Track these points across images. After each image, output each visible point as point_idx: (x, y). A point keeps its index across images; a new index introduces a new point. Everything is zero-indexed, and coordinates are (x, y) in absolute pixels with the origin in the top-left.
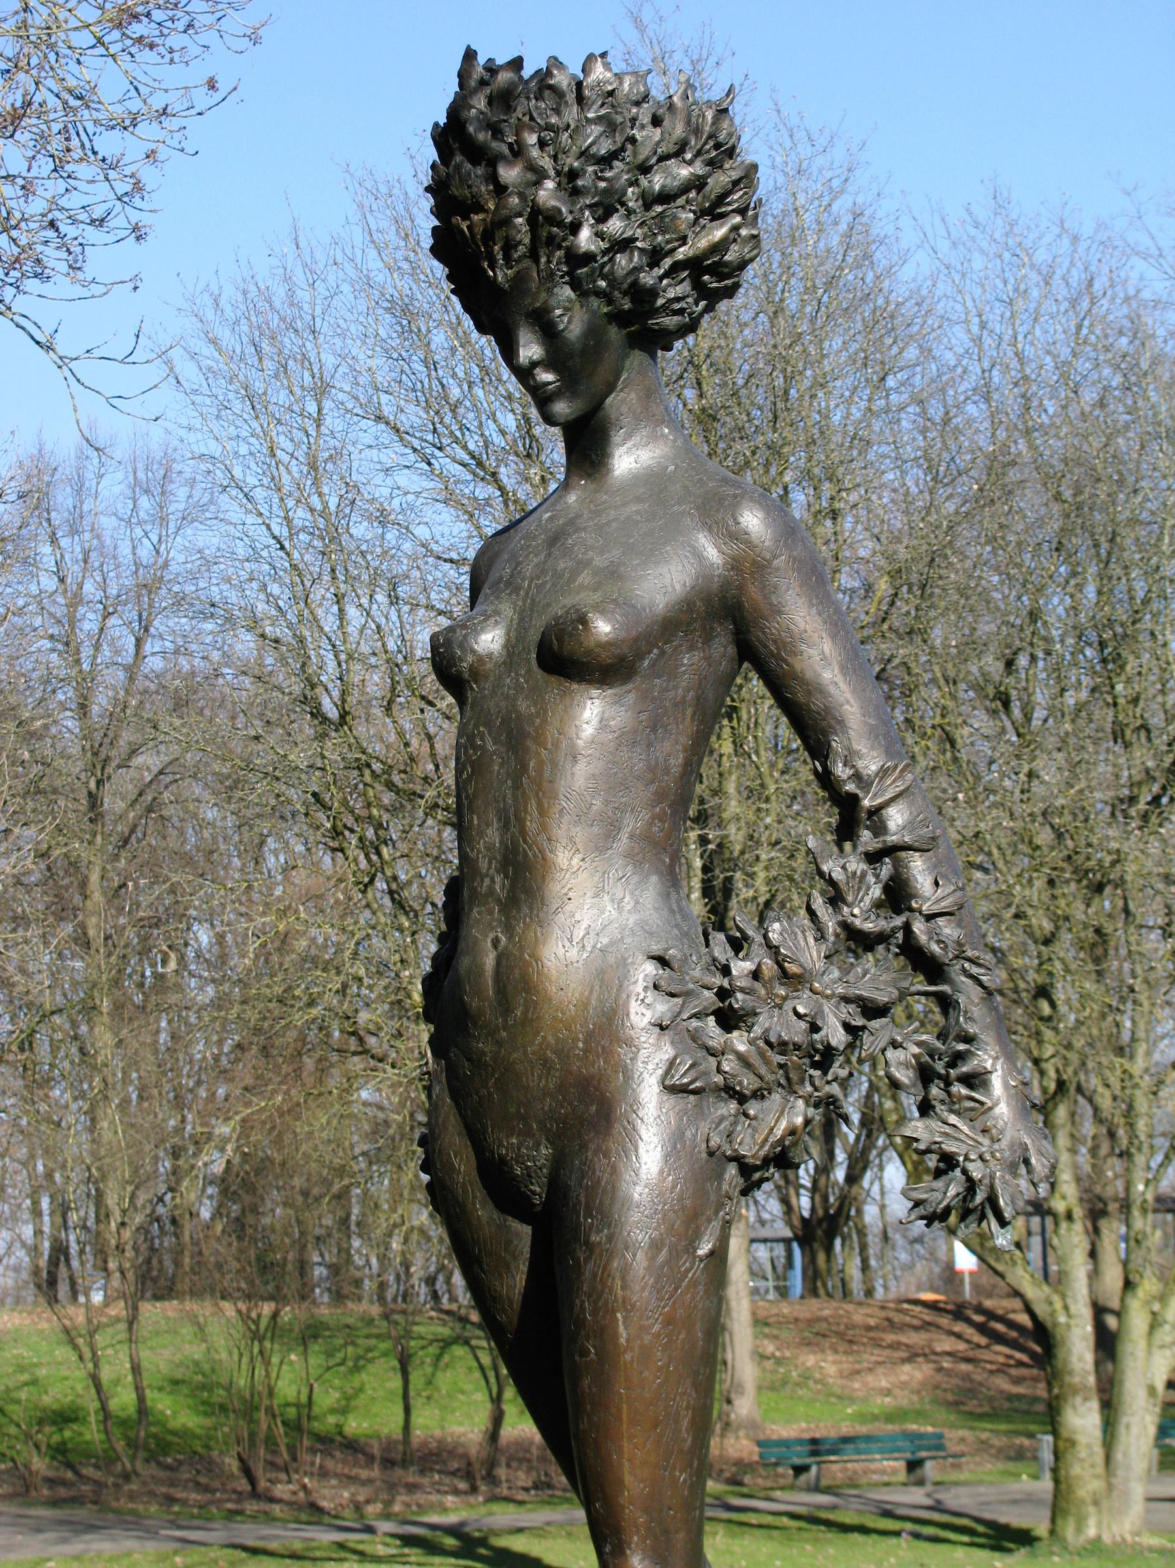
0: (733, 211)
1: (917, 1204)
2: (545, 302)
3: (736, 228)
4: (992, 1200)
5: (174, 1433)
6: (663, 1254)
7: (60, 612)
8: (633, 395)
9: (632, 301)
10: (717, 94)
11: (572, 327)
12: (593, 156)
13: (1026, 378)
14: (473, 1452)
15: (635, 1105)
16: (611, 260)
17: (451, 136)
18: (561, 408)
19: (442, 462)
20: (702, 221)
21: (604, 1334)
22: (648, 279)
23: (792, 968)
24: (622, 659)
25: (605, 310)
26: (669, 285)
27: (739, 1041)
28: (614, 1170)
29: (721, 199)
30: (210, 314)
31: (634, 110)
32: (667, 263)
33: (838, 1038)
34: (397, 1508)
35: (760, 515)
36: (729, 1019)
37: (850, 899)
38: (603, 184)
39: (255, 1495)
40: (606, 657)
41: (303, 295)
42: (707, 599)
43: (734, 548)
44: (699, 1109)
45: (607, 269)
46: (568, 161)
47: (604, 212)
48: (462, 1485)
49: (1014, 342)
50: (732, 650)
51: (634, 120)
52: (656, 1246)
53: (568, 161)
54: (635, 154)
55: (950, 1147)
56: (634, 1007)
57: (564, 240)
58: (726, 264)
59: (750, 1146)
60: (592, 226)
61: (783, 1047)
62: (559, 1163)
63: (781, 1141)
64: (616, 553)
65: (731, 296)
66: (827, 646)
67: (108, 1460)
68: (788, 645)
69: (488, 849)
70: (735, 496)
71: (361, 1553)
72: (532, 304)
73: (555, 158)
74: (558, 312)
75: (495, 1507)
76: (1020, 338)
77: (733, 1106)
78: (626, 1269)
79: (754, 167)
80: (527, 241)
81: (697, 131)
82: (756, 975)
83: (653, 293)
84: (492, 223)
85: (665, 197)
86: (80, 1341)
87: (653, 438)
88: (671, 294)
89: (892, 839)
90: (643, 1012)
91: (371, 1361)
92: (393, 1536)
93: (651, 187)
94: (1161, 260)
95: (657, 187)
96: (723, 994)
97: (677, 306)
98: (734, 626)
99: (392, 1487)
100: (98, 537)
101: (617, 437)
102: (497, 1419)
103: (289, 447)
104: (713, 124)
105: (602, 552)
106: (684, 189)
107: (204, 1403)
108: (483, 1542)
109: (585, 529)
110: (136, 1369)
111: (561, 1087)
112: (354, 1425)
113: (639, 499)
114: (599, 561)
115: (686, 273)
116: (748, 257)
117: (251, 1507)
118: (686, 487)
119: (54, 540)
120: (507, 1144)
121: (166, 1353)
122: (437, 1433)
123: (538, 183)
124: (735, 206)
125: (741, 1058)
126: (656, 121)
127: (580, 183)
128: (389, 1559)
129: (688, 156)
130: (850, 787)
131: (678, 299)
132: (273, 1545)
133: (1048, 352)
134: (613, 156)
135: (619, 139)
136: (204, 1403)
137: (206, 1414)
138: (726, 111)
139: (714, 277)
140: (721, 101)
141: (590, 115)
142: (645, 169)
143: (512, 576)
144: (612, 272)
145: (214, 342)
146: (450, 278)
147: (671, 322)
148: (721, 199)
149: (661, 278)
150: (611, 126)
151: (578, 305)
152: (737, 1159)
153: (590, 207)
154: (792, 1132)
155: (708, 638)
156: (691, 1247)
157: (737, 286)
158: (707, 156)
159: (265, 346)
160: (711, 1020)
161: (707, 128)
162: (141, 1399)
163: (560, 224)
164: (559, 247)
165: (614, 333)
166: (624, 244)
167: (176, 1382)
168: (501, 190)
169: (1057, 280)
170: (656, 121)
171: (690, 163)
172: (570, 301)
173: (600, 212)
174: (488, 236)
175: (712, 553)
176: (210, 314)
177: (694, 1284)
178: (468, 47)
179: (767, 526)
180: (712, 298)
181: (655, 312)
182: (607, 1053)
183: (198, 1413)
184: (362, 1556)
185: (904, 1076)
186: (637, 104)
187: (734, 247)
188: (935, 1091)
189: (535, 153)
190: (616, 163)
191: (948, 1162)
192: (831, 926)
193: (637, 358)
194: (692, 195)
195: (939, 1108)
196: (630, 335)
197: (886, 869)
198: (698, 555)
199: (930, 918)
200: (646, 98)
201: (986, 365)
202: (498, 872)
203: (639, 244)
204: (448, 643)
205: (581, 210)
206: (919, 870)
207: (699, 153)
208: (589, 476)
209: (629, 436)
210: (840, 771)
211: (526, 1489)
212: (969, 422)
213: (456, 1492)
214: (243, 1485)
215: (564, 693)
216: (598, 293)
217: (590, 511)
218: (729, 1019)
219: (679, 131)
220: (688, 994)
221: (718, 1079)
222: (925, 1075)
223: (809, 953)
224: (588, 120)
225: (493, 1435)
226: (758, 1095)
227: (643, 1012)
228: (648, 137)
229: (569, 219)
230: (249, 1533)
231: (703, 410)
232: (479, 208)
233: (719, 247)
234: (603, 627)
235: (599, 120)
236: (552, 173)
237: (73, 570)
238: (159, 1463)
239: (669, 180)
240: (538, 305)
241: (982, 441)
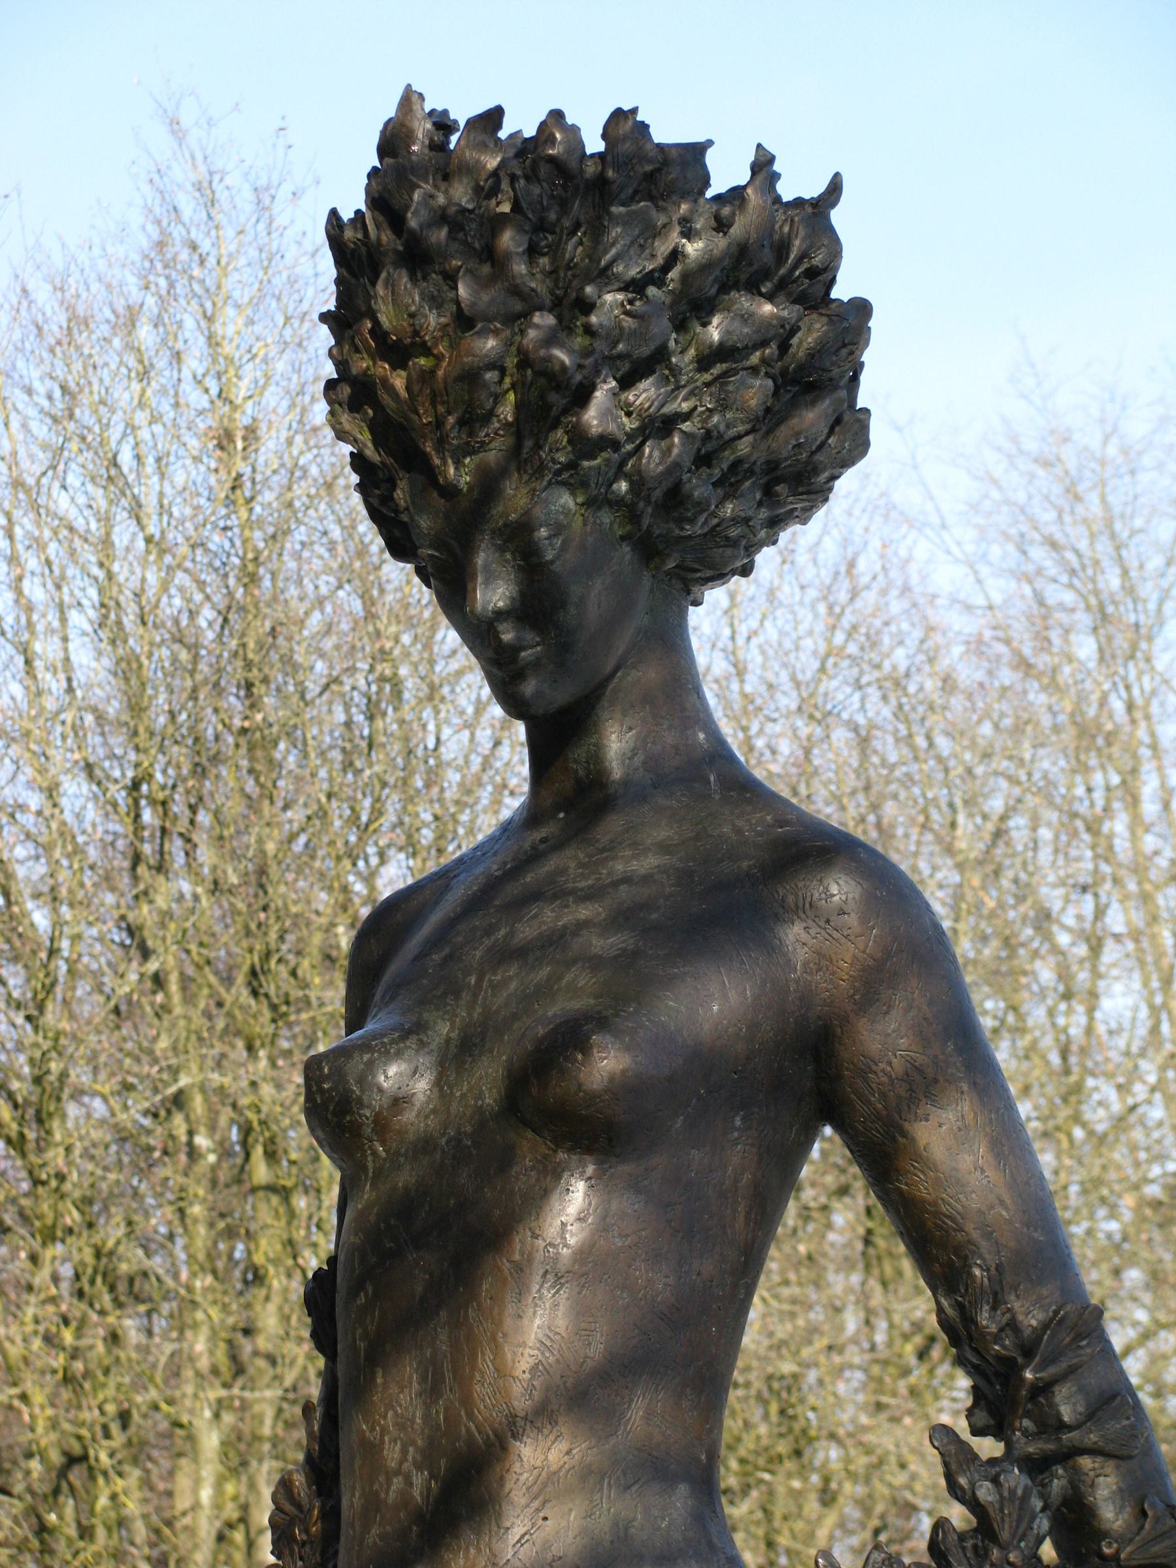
2: (527, 513)
10: (813, 189)
16: (639, 448)
37: (1005, 1535)
69: (401, 1427)
74: (543, 532)
94: (944, 533)
202: (419, 1467)
204: (339, 1074)
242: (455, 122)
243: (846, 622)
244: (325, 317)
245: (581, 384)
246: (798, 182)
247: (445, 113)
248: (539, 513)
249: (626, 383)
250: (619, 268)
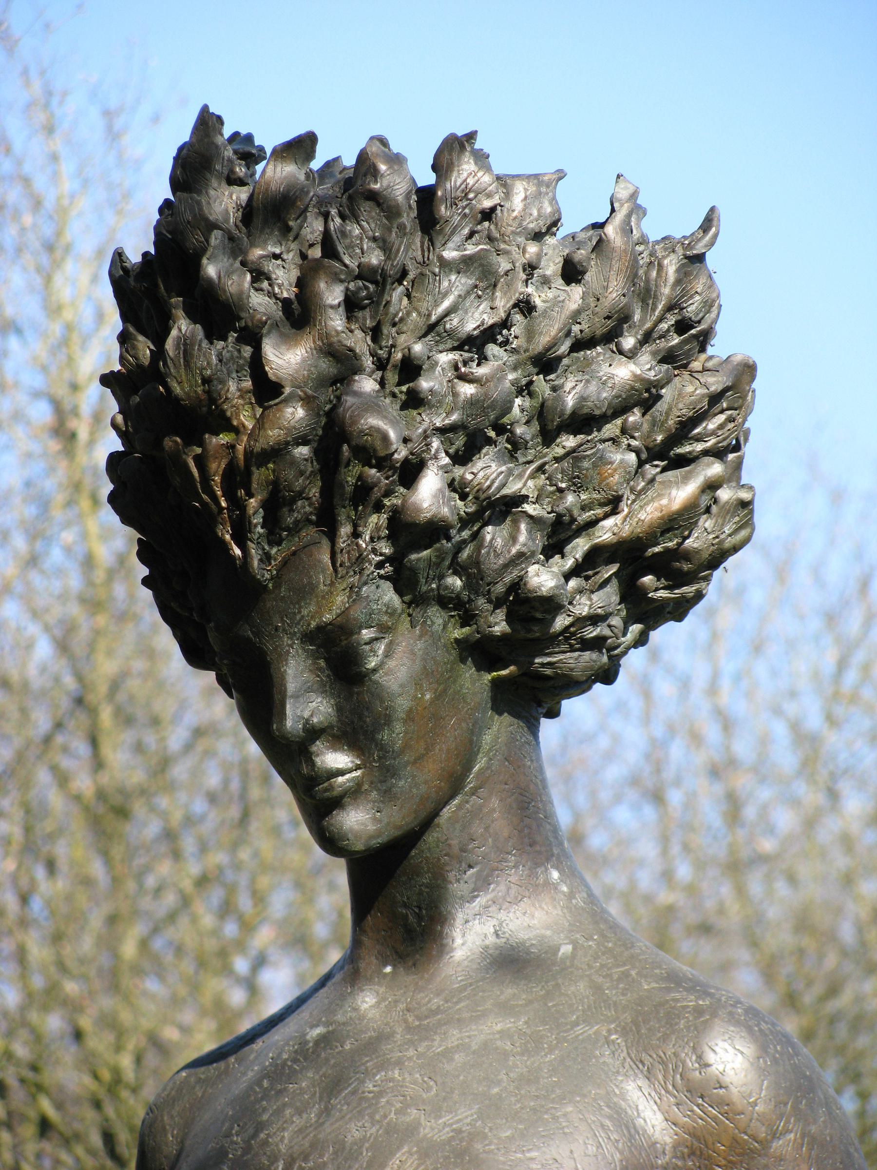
0: (706, 453)
2: (345, 612)
3: (712, 486)
8: (495, 802)
9: (509, 620)
10: (685, 226)
11: (391, 664)
12: (450, 334)
13: (732, 763)
16: (476, 536)
17: (158, 286)
18: (357, 821)
20: (650, 470)
22: (543, 578)
25: (458, 633)
26: (580, 591)
29: (685, 429)
31: (532, 249)
32: (579, 547)
35: (749, 1049)
38: (467, 390)
43: (695, 1114)
45: (465, 554)
46: (402, 339)
47: (468, 443)
49: (713, 690)
51: (531, 268)
53: (402, 339)
54: (530, 334)
57: (388, 493)
58: (687, 556)
60: (445, 470)
64: (464, 1115)
65: (680, 618)
70: (699, 1011)
72: (319, 613)
73: (376, 333)
74: (367, 634)
76: (726, 684)
79: (748, 370)
80: (314, 492)
83: (551, 605)
84: (249, 454)
85: (584, 422)
88: (583, 607)
93: (560, 400)
95: (570, 401)
97: (591, 632)
104: (678, 282)
105: (436, 1112)
109: (399, 1063)
115: (613, 568)
116: (729, 543)
118: (597, 989)
124: (711, 442)
126: (572, 273)
127: (425, 384)
129: (628, 342)
131: (594, 619)
133: (777, 711)
135: (503, 302)
138: (700, 258)
139: (660, 577)
140: (693, 239)
141: (450, 254)
142: (546, 364)
143: (247, 1149)
144: (476, 561)
146: (145, 554)
148: (685, 429)
149: (567, 577)
151: (405, 621)
153: (442, 431)
157: (699, 596)
158: (662, 344)
161: (666, 291)
163: (383, 462)
164: (378, 507)
165: (475, 683)
166: (504, 508)
168: (267, 390)
169: (801, 576)
170: (572, 273)
171: (631, 355)
172: (391, 612)
173: (460, 441)
178: (205, 109)
179: (762, 1072)
180: (648, 614)
181: (548, 642)
186: (538, 236)
187: (706, 523)
190: (492, 349)
194: (635, 417)
196: (497, 685)
198: (625, 1123)
201: (658, 731)
203: (529, 508)
205: (425, 436)
207: (647, 338)
209: (483, 883)
212: (624, 842)
216: (445, 601)
217: (409, 1029)
219: (615, 292)
224: (445, 264)
228: (556, 303)
229: (401, 453)
231: (101, 795)
233: (678, 522)
235: (466, 264)
236: (368, 362)
239: (593, 388)
240: (327, 617)
241: (646, 880)
242: (261, 149)
243: (859, 657)
244: (107, 380)
245: (406, 461)
246: (668, 219)
247: (249, 138)
248: (358, 613)
249: (462, 458)
250: (453, 322)
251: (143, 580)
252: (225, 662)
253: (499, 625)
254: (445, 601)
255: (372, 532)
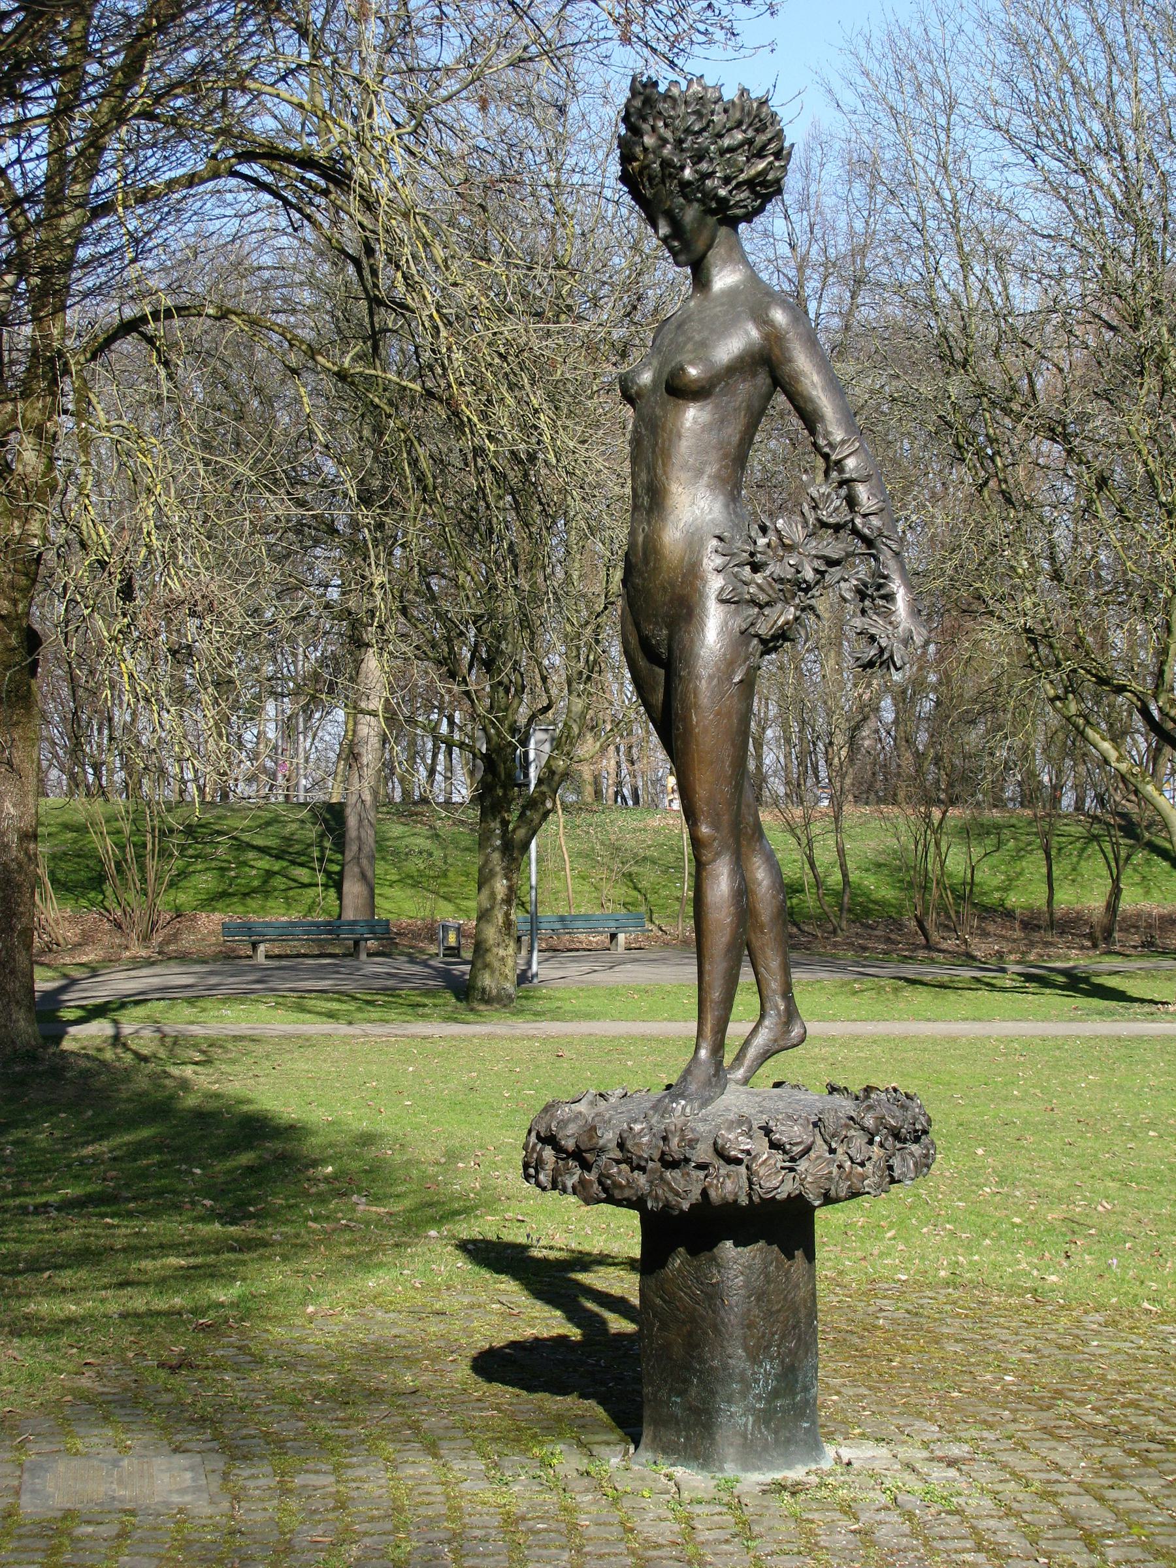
1: (858, 659)
3: (771, 163)
4: (892, 657)
5: (875, 902)
6: (715, 682)
7: (792, 273)
14: (1095, 919)
15: (704, 609)
19: (1044, 159)
21: (686, 719)
22: (722, 192)
23: (787, 541)
24: (703, 388)
27: (759, 578)
28: (692, 641)
30: (863, 52)
32: (734, 183)
33: (809, 575)
34: (1032, 957)
36: (756, 568)
39: (928, 947)
40: (694, 387)
41: (936, 33)
42: (752, 356)
44: (737, 612)
48: (1089, 944)
50: (769, 381)
52: (711, 677)
55: (873, 631)
56: (705, 561)
59: (763, 629)
61: (780, 580)
62: (671, 638)
63: (781, 627)
64: (706, 334)
66: (816, 378)
67: (821, 919)
68: (795, 378)
71: (992, 985)
75: (1107, 959)
77: (756, 610)
78: (696, 687)
81: (749, 114)
82: (769, 545)
85: (731, 150)
86: (798, 832)
87: (734, 271)
89: (847, 476)
90: (711, 561)
91: (1031, 852)
92: (1019, 974)
96: (752, 555)
98: (768, 366)
99: (1032, 944)
100: (821, 214)
101: (714, 271)
102: (1116, 892)
103: (923, 150)
106: (741, 145)
107: (901, 881)
108: (1086, 980)
110: (841, 852)
111: (671, 601)
112: (1014, 900)
113: (722, 304)
114: (697, 337)
117: (921, 954)
119: (787, 217)
120: (648, 629)
121: (873, 844)
122: (1078, 907)
123: (663, 146)
125: (759, 586)
128: (1013, 990)
130: (827, 450)
132: (927, 979)
134: (703, 130)
135: (704, 122)
136: (901, 881)
137: (901, 889)
139: (766, 190)
145: (866, 74)
147: (739, 212)
150: (698, 113)
152: (757, 636)
154: (787, 623)
155: (754, 375)
156: (730, 678)
159: (907, 74)
160: (748, 568)
162: (845, 875)
163: (674, 167)
166: (710, 175)
167: (879, 865)
174: (641, 173)
175: (755, 333)
176: (863, 52)
177: (731, 696)
181: (731, 208)
182: (692, 584)
183: (894, 887)
184: (992, 987)
185: (848, 596)
188: (867, 603)
189: (662, 130)
191: (873, 638)
192: (811, 521)
193: (723, 231)
195: (870, 612)
197: (843, 492)
198: (747, 333)
199: (865, 516)
200: (720, 98)
206: (862, 491)
208: (701, 291)
210: (822, 442)
211: (1135, 947)
213: (1082, 948)
214: (921, 940)
215: (676, 405)
216: (698, 200)
218: (756, 568)
219: (738, 115)
220: (733, 555)
221: (747, 597)
222: (861, 594)
223: (797, 533)
225: (1112, 907)
226: (768, 604)
227: (711, 561)
230: (910, 971)
232: (636, 160)
233: (764, 172)
234: (693, 371)
235: (694, 113)
237: (802, 239)
238: (862, 924)
246: (756, 93)
251: (475, 1360)
252: (64, 24)
253: (714, 205)
254: (698, 200)
255: (674, 186)
